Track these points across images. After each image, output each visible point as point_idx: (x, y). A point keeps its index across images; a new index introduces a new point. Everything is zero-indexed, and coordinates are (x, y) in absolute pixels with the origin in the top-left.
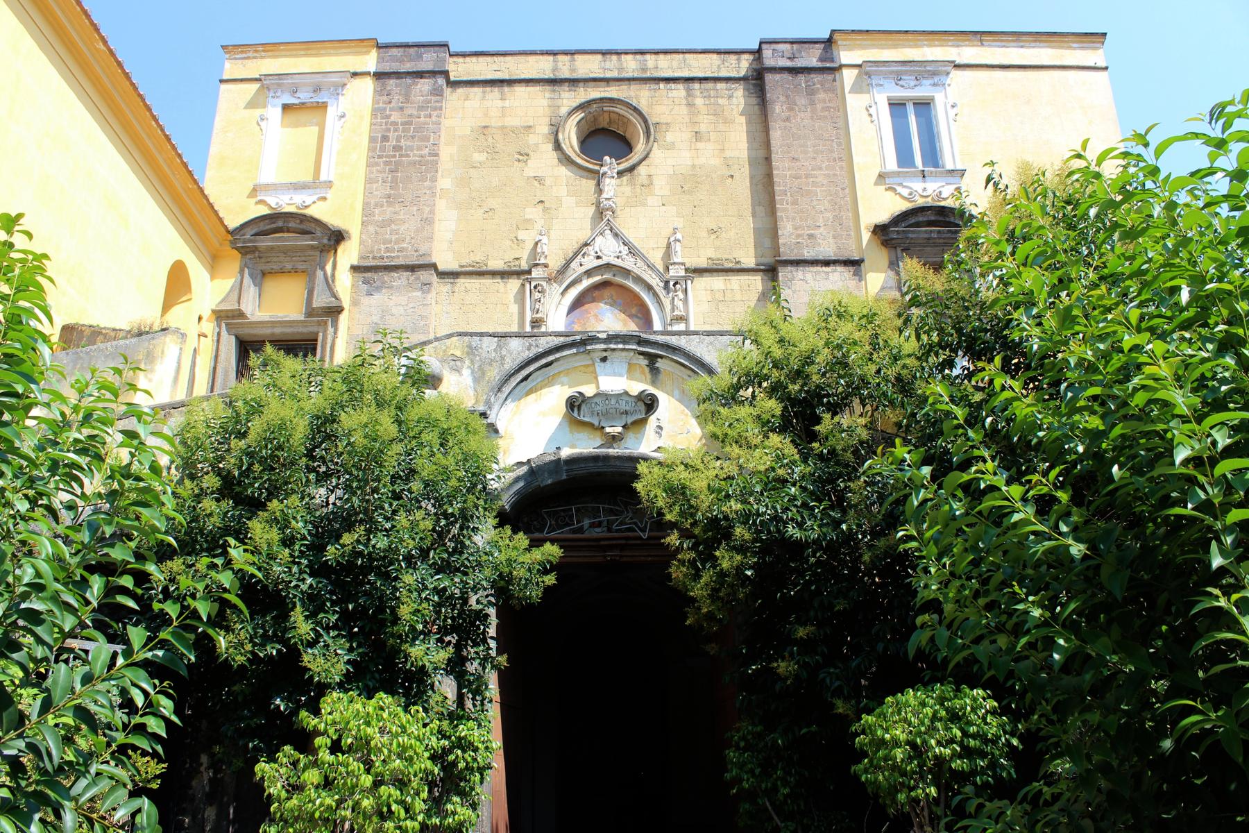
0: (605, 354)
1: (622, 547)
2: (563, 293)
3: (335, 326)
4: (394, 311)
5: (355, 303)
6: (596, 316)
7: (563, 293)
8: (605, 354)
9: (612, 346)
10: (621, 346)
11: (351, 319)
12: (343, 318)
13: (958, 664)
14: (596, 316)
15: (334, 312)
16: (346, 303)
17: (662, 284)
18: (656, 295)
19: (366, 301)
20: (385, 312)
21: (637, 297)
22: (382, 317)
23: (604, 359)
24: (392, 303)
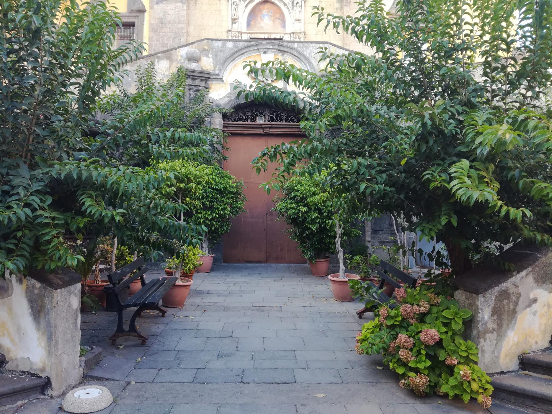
0: (265, 50)
1: (270, 128)
2: (246, 6)
3: (144, 15)
4: (170, 12)
5: (151, 8)
6: (261, 18)
7: (246, 6)
8: (265, 50)
9: (268, 47)
10: (271, 47)
11: (150, 16)
12: (146, 14)
13: (390, 187)
14: (261, 18)
15: (142, 11)
16: (147, 8)
17: (291, 3)
18: (288, 8)
19: (156, 7)
20: (165, 13)
21: (279, 8)
22: (164, 15)
23: (265, 52)
24: (168, 8)
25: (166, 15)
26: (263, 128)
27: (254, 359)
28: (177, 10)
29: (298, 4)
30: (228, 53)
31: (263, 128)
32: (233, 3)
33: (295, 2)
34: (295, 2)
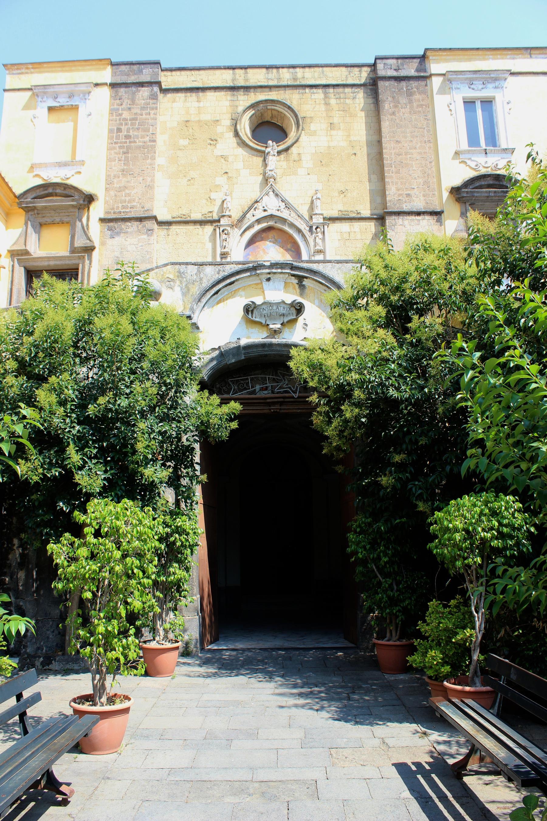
0: (269, 276)
1: (281, 403)
3: (443, 701)
5: (103, 244)
6: (264, 250)
8: (269, 276)
9: (274, 271)
12: (95, 254)
14: (264, 250)
15: (89, 250)
16: (97, 244)
17: (308, 229)
18: (303, 236)
19: (110, 242)
21: (291, 237)
22: (121, 253)
23: (268, 280)
25: (124, 253)
26: (270, 404)
27: (389, 221)
28: (140, 244)
29: (318, 230)
30: (206, 284)
31: (270, 404)
32: (223, 231)
33: (314, 227)
34: (314, 227)
